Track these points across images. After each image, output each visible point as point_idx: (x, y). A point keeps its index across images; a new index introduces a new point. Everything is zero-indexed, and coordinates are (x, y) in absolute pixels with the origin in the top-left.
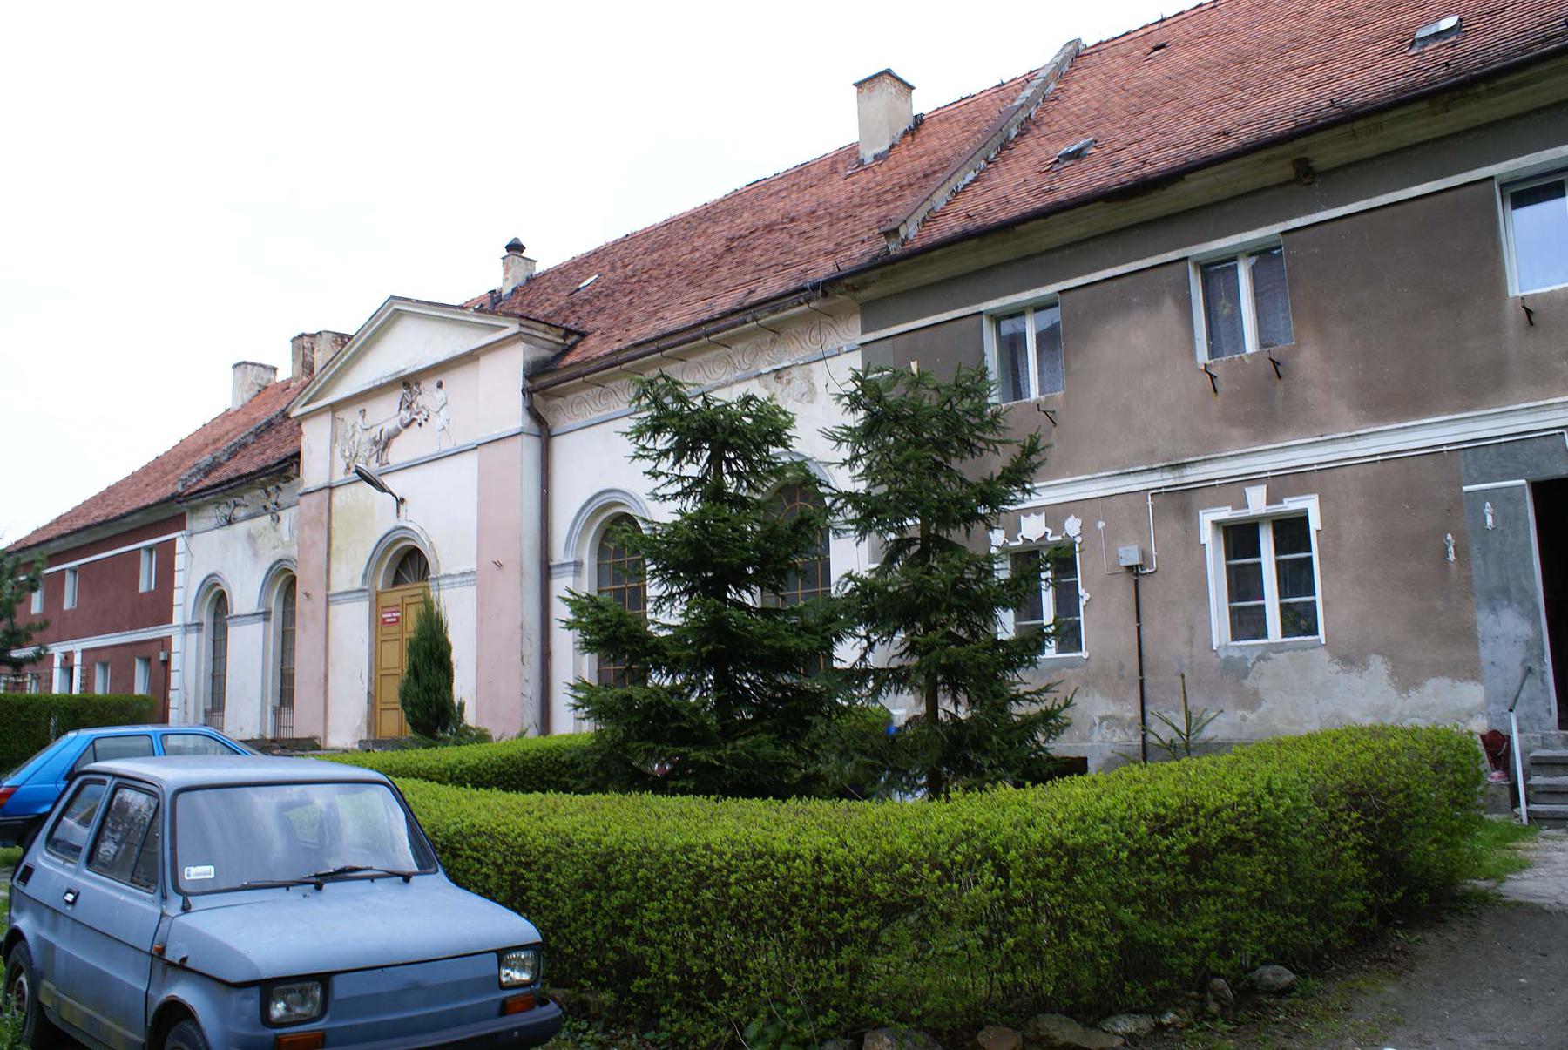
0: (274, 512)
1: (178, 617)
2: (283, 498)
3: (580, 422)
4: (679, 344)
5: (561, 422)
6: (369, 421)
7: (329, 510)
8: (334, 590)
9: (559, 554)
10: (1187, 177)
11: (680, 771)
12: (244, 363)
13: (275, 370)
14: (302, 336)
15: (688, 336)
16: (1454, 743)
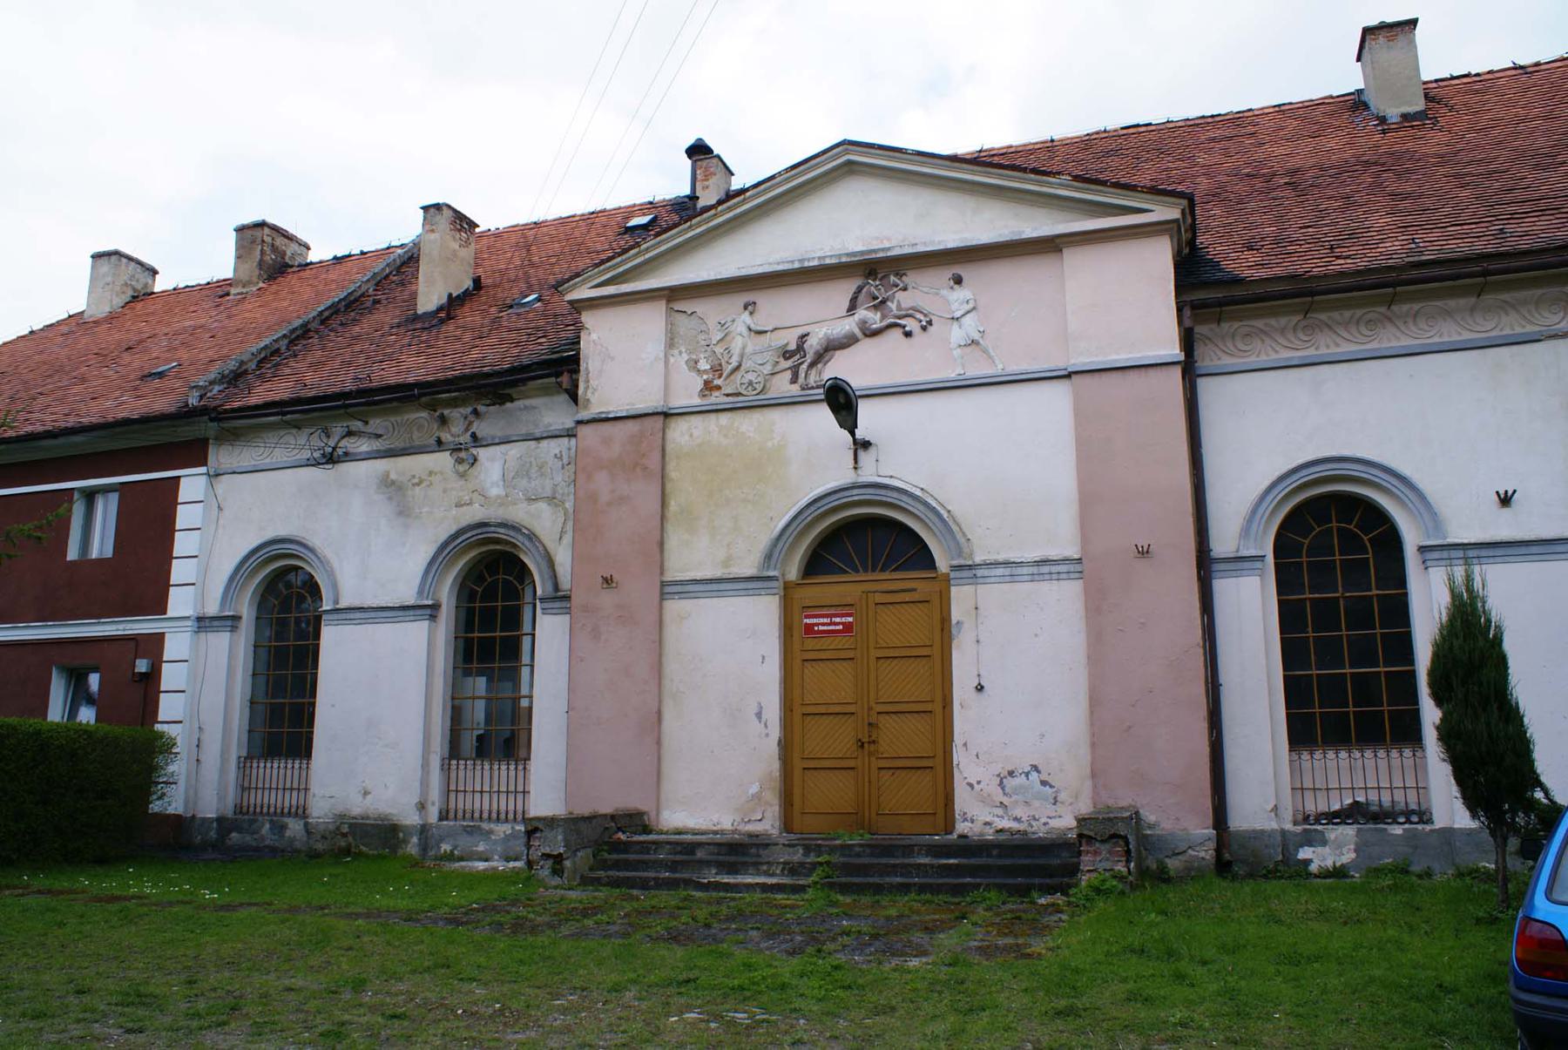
0: (465, 453)
1: (180, 602)
2: (482, 428)
3: (1252, 360)
4: (1517, 270)
5: (1207, 358)
6: (762, 320)
7: (663, 450)
8: (668, 577)
9: (1224, 542)
10: (911, 278)
11: (693, 853)
12: (116, 253)
13: (154, 272)
14: (262, 225)
15: (1536, 261)
16: (345, 829)
